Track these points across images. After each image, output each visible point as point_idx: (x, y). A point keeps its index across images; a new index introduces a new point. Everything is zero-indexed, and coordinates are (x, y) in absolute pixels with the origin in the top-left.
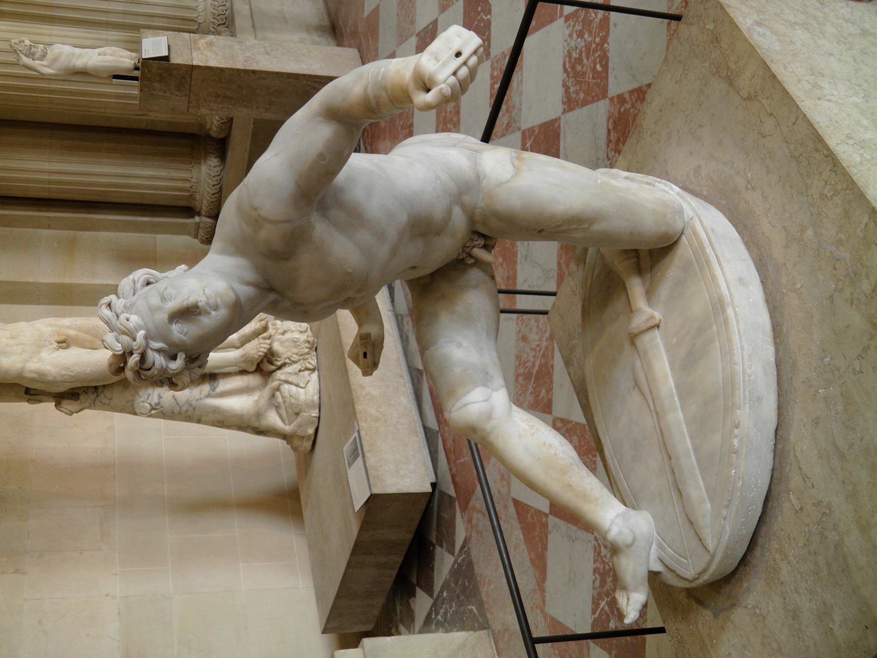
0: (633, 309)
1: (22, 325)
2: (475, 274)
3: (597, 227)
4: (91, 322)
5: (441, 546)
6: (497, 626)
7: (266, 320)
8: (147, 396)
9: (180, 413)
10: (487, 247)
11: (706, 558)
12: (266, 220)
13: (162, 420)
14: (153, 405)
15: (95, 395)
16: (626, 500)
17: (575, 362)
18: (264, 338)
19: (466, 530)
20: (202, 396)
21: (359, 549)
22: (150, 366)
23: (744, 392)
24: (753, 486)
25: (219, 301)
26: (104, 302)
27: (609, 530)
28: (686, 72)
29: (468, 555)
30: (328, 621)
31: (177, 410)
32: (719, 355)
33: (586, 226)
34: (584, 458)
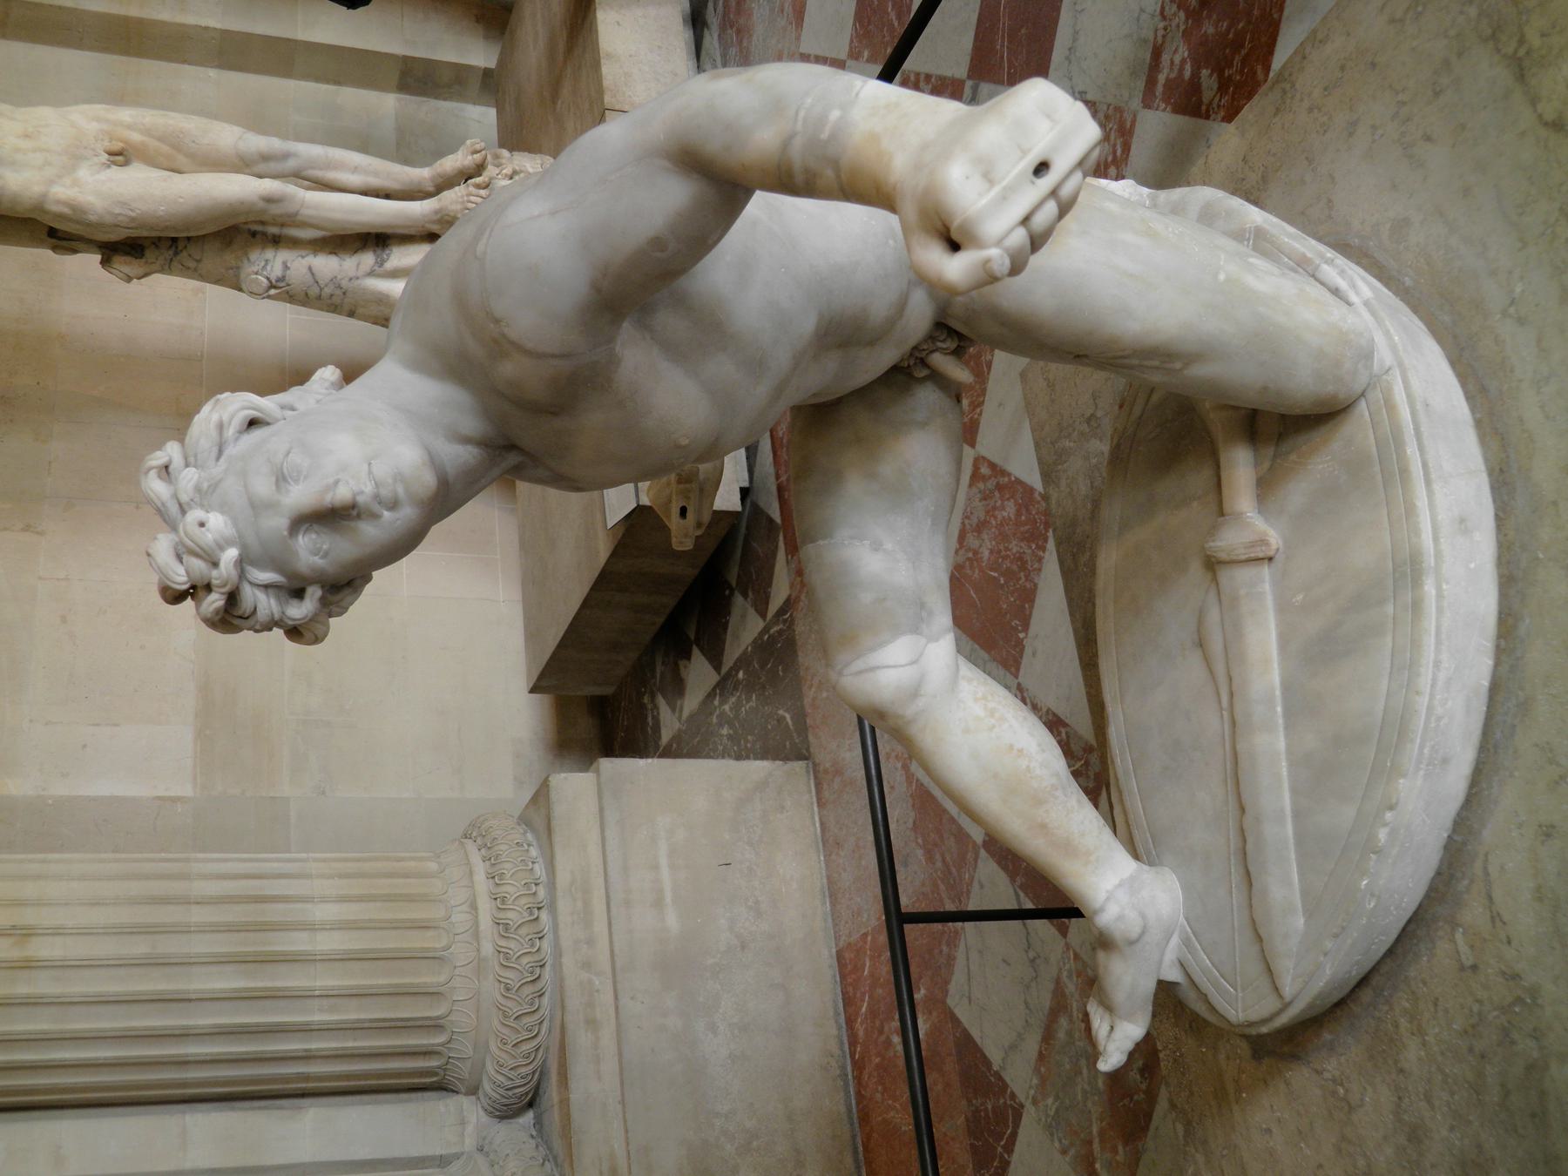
0: (1227, 507)
1: (45, 113)
2: (927, 397)
3: (1200, 371)
4: (171, 122)
5: (745, 595)
6: (823, 758)
7: (483, 152)
8: (263, 264)
9: (319, 297)
10: (958, 353)
11: (1277, 1005)
12: (518, 347)
13: (288, 305)
14: (273, 281)
15: (171, 252)
16: (1141, 850)
17: (1063, 483)
18: (478, 186)
19: (792, 586)
20: (360, 273)
21: (605, 581)
22: (252, 609)
23: (1422, 747)
24: (1392, 908)
25: (400, 490)
26: (155, 463)
27: (1102, 910)
28: (1420, 9)
29: (789, 627)
30: (542, 675)
31: (314, 291)
32: (1388, 665)
33: (1178, 365)
34: (1022, 544)
